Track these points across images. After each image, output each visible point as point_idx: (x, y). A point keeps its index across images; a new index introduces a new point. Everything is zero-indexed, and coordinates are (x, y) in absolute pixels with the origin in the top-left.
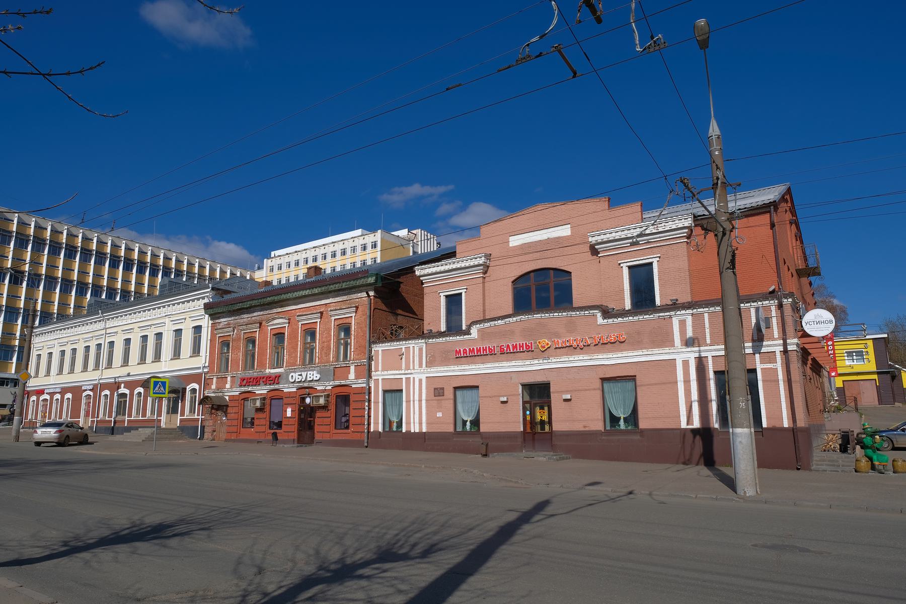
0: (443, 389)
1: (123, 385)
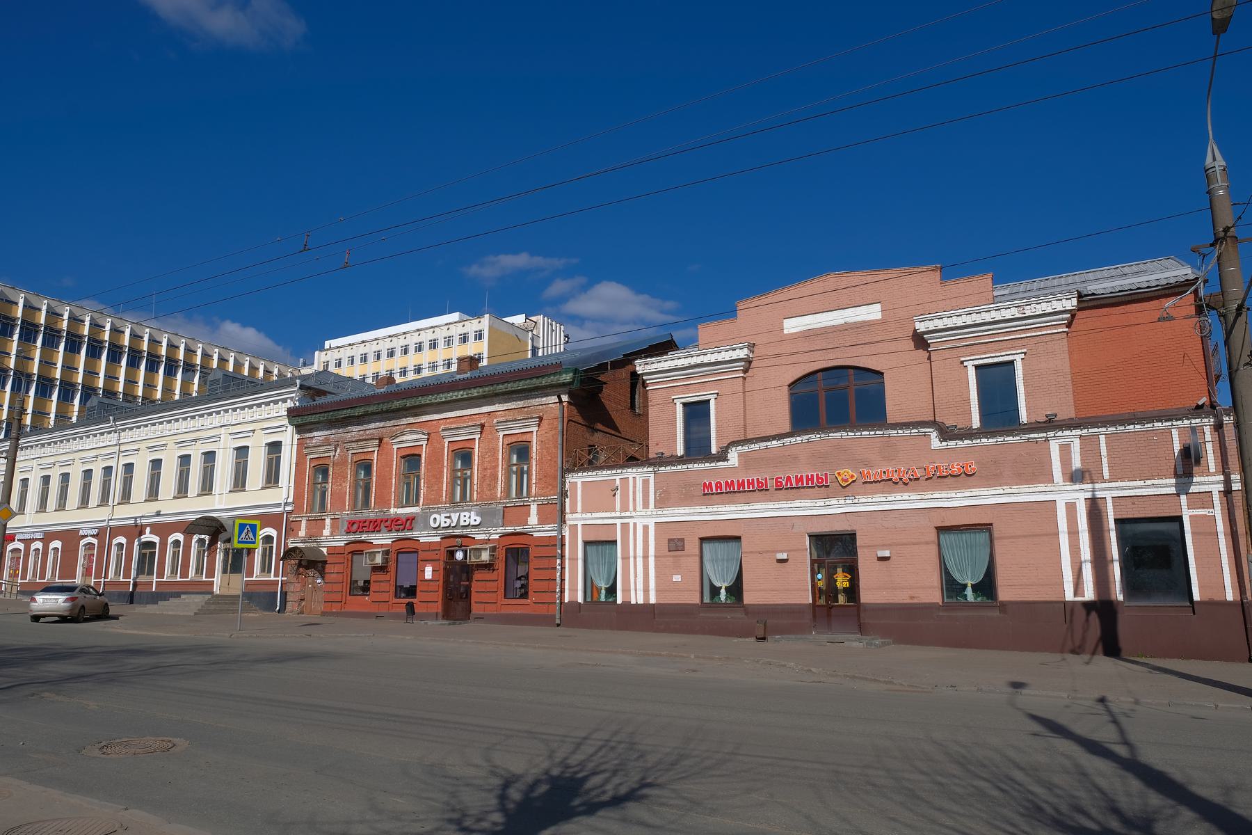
1: (148, 530)
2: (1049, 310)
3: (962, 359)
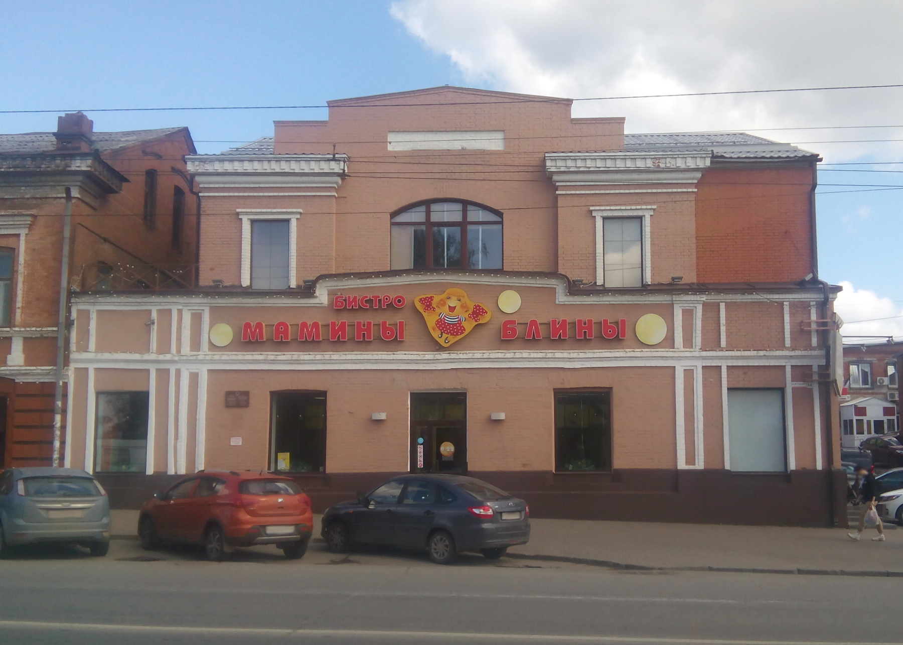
0: (246, 393)
2: (240, 170)
3: (592, 208)
